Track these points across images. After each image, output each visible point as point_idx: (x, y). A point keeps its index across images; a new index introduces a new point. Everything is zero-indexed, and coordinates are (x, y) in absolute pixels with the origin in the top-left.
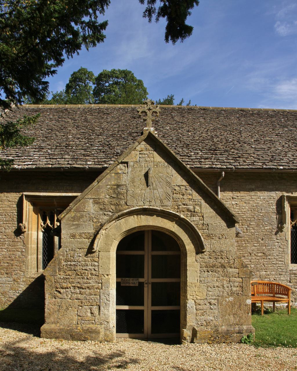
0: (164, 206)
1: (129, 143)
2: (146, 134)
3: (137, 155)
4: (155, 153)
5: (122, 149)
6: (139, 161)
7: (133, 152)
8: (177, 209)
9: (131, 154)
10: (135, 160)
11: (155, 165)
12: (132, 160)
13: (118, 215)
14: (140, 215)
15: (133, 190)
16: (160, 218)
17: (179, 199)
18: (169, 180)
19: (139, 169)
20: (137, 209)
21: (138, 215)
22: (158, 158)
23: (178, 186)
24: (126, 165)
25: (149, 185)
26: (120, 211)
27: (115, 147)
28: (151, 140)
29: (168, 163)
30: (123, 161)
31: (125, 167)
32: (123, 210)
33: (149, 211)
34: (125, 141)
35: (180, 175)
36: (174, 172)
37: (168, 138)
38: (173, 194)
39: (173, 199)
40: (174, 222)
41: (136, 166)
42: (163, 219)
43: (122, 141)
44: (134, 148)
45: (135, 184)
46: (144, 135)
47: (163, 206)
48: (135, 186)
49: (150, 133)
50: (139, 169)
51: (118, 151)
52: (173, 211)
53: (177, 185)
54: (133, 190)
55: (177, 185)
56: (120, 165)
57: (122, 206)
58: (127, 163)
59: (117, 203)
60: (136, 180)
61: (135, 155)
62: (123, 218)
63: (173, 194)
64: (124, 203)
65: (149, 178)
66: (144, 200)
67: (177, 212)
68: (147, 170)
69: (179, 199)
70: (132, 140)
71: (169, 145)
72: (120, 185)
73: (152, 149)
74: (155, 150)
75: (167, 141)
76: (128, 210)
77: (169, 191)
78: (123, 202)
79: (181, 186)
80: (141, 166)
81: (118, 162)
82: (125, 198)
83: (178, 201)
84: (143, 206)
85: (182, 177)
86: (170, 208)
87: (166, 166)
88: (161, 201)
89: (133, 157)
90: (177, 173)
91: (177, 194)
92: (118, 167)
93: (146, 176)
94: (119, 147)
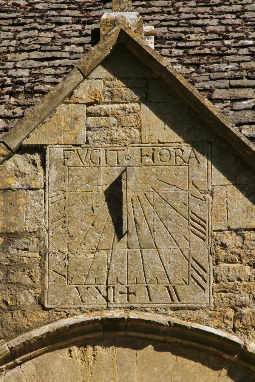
0: (182, 308)
1: (64, 36)
2: (109, 41)
3: (76, 119)
4: (146, 111)
5: (37, 64)
6: (87, 142)
7: (63, 107)
8: (235, 318)
9: (54, 117)
10: (69, 138)
11: (144, 153)
12: (59, 138)
13: (11, 349)
14: (93, 346)
15: (66, 250)
16: (168, 355)
17: (239, 280)
18: (198, 209)
19: (86, 172)
20: (83, 323)
21: (85, 346)
22: (157, 129)
23: (236, 231)
24: (37, 157)
25: (124, 230)
26: (19, 331)
27: (9, 56)
28: (128, 60)
29: (195, 145)
30: (26, 142)
31: (35, 164)
32: (31, 329)
33: (125, 329)
34: (49, 26)
35: (242, 190)
36: (218, 177)
37: (223, 8)
38: (217, 262)
39: (217, 282)
40: (224, 372)
41: (73, 158)
42: (180, 359)
43: (34, 29)
44: (66, 93)
45: (72, 229)
46: (101, 44)
47: (178, 309)
48: (71, 237)
49: (122, 33)
50: (86, 172)
51: (20, 72)
52: (218, 327)
53: (229, 229)
54: (66, 250)
55: (229, 229)
56: (17, 157)
57: (24, 313)
58: (41, 150)
59: (6, 303)
60: (76, 212)
61: (69, 120)
62: (30, 358)
63: (217, 262)
64: (32, 300)
65: (124, 206)
66: (107, 288)
67: (234, 329)
68: (117, 175)
69: (239, 280)
70: (78, 23)
71: (228, 38)
72: (16, 233)
73: (135, 96)
74: (145, 100)
75: (220, 24)
76: (46, 329)
77: (201, 251)
78: (27, 298)
79: (246, 230)
80: (95, 163)
81: (9, 148)
82: (37, 280)
83: (234, 290)
84: (102, 310)
85: (248, 197)
86: (206, 317)
87: (186, 156)
88: (172, 291)
89: (62, 126)
90: (228, 182)
91: (233, 261)
92: (9, 168)
93: (114, 196)
94: (25, 55)
